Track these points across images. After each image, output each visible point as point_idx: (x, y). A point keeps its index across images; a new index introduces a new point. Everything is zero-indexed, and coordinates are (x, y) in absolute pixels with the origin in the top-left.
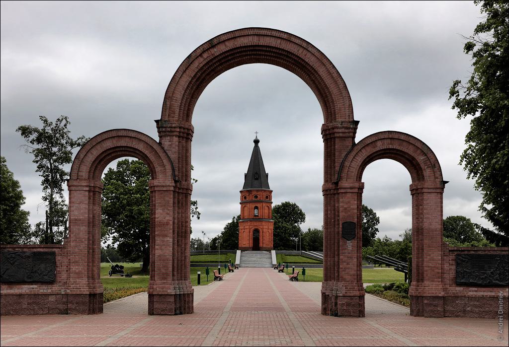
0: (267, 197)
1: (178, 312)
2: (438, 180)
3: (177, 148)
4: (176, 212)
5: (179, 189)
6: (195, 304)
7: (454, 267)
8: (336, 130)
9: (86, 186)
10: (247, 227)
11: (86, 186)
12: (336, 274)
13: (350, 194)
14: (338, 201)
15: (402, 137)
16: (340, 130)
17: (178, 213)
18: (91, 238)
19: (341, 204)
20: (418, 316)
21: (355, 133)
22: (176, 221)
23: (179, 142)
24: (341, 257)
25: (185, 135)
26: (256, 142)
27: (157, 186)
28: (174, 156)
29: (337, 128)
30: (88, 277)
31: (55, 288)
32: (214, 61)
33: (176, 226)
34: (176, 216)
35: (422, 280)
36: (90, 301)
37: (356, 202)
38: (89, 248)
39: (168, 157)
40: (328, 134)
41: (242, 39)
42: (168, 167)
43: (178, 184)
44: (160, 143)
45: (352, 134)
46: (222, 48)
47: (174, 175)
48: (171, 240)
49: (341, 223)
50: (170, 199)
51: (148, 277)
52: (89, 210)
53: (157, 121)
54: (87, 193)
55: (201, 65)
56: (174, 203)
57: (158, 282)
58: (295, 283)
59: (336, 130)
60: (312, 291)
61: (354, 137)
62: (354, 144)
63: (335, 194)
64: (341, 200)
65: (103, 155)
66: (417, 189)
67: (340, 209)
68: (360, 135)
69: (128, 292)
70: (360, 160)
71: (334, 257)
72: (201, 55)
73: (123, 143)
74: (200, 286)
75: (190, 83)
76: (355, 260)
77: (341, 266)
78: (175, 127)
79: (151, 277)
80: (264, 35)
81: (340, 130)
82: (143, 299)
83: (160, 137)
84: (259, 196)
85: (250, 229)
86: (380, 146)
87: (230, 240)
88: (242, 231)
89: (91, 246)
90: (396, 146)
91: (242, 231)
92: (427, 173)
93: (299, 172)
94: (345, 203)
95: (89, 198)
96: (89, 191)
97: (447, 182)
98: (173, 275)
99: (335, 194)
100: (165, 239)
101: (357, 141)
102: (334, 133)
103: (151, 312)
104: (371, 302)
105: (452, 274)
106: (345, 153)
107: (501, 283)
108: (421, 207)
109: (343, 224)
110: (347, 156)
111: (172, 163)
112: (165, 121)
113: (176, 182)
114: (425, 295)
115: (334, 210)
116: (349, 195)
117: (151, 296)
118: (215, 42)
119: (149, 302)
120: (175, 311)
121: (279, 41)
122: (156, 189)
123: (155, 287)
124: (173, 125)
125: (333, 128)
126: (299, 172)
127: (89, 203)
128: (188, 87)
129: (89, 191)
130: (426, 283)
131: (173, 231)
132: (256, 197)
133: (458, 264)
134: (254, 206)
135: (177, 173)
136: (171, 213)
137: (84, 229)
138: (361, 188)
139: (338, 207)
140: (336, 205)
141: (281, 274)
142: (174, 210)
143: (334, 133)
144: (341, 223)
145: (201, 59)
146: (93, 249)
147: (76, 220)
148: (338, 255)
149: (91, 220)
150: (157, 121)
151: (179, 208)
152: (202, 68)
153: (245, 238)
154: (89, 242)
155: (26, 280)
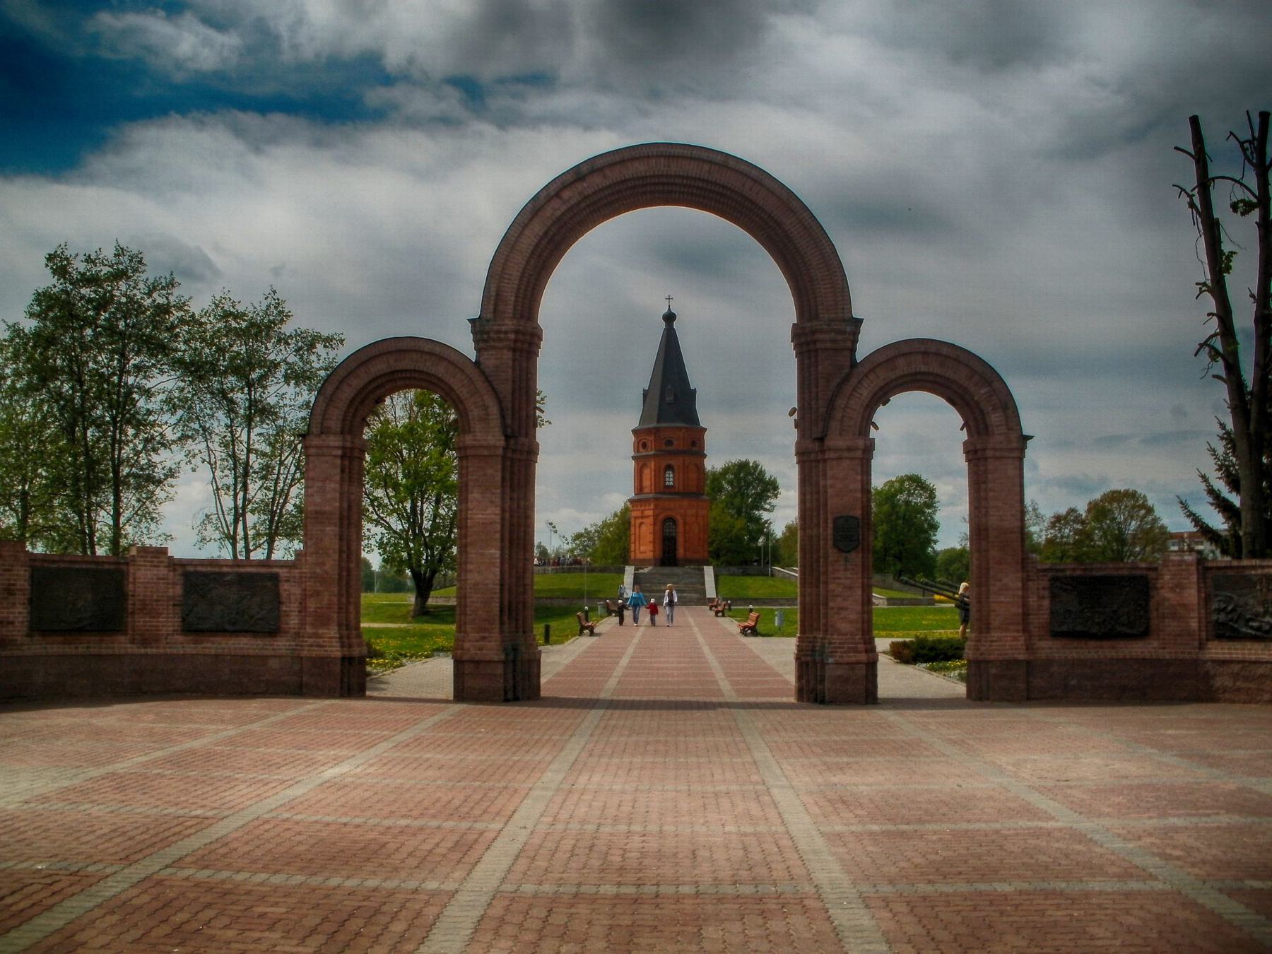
0: (694, 444)
1: (510, 695)
2: (1013, 436)
3: (510, 370)
4: (507, 497)
5: (514, 451)
6: (543, 680)
7: (1046, 603)
8: (818, 336)
9: (338, 448)
10: (650, 513)
11: (338, 448)
12: (822, 621)
13: (848, 462)
14: (825, 475)
15: (945, 351)
16: (826, 337)
17: (511, 499)
18: (345, 548)
19: (830, 482)
20: (980, 699)
21: (855, 341)
22: (507, 515)
23: (514, 360)
24: (831, 586)
25: (526, 346)
26: (670, 318)
27: (473, 447)
28: (505, 389)
29: (822, 331)
30: (340, 625)
31: (282, 645)
32: (583, 205)
33: (507, 524)
34: (507, 505)
35: (988, 629)
36: (342, 672)
37: (859, 478)
38: (341, 569)
39: (494, 389)
40: (804, 340)
41: (636, 164)
42: (494, 410)
43: (512, 442)
44: (477, 363)
45: (849, 344)
46: (598, 181)
47: (504, 426)
48: (497, 553)
49: (830, 517)
50: (494, 472)
51: (454, 627)
52: (341, 494)
53: (472, 321)
54: (338, 462)
55: (558, 213)
56: (503, 479)
57: (474, 636)
58: (753, 642)
59: (818, 336)
60: (779, 655)
61: (853, 350)
62: (854, 364)
63: (818, 461)
64: (829, 473)
65: (373, 385)
66: (976, 452)
67: (829, 490)
68: (866, 345)
69: (417, 653)
70: (865, 392)
71: (818, 587)
72: (557, 195)
73: (406, 363)
74: (549, 647)
75: (537, 245)
76: (859, 592)
77: (831, 604)
78: (506, 333)
79: (459, 627)
80: (678, 157)
81: (826, 337)
82: (443, 667)
83: (478, 350)
84: (675, 442)
85: (655, 517)
86: (902, 367)
87: (610, 547)
88: (638, 521)
89: (344, 565)
90: (934, 367)
91: (638, 521)
92: (995, 418)
93: (753, 429)
94: (838, 477)
95: (343, 471)
96: (343, 457)
97: (1030, 437)
98: (502, 623)
99: (818, 461)
100: (487, 552)
101: (860, 355)
102: (815, 342)
103: (462, 694)
104: (894, 678)
105: (1044, 617)
106: (838, 380)
107: (1129, 631)
108: (983, 486)
109: (835, 520)
110: (840, 386)
111: (500, 402)
112: (488, 321)
113: (507, 437)
114: (992, 657)
115: (818, 493)
116: (846, 463)
117: (458, 663)
118: (585, 169)
119: (456, 675)
120: (506, 693)
121: (706, 167)
122: (470, 452)
123: (467, 645)
124: (504, 328)
125: (813, 332)
126: (753, 429)
127: (342, 480)
128: (533, 253)
129: (343, 457)
130: (995, 635)
131: (502, 535)
132: (669, 443)
133: (1053, 597)
134: (664, 463)
135: (509, 421)
136: (498, 501)
137: (332, 529)
138: (869, 449)
139: (825, 486)
140: (822, 483)
141: (721, 620)
142: (503, 493)
143: (815, 342)
144: (830, 517)
145: (556, 203)
146: (348, 570)
147: (317, 512)
148: (826, 583)
149: (345, 514)
150: (472, 321)
151: (512, 490)
152: (559, 219)
153: (315, 430)
154: (340, 556)
155: (228, 627)
